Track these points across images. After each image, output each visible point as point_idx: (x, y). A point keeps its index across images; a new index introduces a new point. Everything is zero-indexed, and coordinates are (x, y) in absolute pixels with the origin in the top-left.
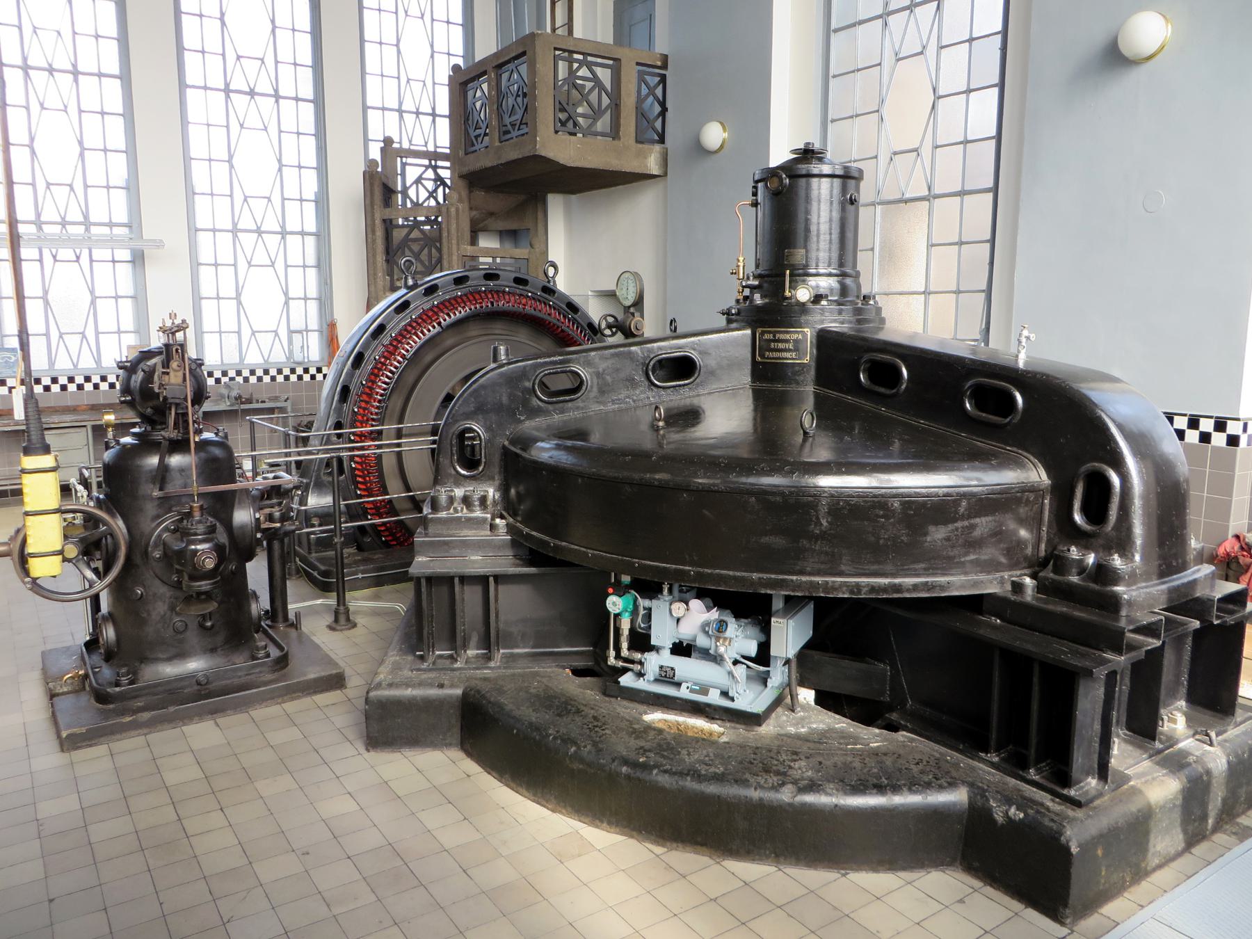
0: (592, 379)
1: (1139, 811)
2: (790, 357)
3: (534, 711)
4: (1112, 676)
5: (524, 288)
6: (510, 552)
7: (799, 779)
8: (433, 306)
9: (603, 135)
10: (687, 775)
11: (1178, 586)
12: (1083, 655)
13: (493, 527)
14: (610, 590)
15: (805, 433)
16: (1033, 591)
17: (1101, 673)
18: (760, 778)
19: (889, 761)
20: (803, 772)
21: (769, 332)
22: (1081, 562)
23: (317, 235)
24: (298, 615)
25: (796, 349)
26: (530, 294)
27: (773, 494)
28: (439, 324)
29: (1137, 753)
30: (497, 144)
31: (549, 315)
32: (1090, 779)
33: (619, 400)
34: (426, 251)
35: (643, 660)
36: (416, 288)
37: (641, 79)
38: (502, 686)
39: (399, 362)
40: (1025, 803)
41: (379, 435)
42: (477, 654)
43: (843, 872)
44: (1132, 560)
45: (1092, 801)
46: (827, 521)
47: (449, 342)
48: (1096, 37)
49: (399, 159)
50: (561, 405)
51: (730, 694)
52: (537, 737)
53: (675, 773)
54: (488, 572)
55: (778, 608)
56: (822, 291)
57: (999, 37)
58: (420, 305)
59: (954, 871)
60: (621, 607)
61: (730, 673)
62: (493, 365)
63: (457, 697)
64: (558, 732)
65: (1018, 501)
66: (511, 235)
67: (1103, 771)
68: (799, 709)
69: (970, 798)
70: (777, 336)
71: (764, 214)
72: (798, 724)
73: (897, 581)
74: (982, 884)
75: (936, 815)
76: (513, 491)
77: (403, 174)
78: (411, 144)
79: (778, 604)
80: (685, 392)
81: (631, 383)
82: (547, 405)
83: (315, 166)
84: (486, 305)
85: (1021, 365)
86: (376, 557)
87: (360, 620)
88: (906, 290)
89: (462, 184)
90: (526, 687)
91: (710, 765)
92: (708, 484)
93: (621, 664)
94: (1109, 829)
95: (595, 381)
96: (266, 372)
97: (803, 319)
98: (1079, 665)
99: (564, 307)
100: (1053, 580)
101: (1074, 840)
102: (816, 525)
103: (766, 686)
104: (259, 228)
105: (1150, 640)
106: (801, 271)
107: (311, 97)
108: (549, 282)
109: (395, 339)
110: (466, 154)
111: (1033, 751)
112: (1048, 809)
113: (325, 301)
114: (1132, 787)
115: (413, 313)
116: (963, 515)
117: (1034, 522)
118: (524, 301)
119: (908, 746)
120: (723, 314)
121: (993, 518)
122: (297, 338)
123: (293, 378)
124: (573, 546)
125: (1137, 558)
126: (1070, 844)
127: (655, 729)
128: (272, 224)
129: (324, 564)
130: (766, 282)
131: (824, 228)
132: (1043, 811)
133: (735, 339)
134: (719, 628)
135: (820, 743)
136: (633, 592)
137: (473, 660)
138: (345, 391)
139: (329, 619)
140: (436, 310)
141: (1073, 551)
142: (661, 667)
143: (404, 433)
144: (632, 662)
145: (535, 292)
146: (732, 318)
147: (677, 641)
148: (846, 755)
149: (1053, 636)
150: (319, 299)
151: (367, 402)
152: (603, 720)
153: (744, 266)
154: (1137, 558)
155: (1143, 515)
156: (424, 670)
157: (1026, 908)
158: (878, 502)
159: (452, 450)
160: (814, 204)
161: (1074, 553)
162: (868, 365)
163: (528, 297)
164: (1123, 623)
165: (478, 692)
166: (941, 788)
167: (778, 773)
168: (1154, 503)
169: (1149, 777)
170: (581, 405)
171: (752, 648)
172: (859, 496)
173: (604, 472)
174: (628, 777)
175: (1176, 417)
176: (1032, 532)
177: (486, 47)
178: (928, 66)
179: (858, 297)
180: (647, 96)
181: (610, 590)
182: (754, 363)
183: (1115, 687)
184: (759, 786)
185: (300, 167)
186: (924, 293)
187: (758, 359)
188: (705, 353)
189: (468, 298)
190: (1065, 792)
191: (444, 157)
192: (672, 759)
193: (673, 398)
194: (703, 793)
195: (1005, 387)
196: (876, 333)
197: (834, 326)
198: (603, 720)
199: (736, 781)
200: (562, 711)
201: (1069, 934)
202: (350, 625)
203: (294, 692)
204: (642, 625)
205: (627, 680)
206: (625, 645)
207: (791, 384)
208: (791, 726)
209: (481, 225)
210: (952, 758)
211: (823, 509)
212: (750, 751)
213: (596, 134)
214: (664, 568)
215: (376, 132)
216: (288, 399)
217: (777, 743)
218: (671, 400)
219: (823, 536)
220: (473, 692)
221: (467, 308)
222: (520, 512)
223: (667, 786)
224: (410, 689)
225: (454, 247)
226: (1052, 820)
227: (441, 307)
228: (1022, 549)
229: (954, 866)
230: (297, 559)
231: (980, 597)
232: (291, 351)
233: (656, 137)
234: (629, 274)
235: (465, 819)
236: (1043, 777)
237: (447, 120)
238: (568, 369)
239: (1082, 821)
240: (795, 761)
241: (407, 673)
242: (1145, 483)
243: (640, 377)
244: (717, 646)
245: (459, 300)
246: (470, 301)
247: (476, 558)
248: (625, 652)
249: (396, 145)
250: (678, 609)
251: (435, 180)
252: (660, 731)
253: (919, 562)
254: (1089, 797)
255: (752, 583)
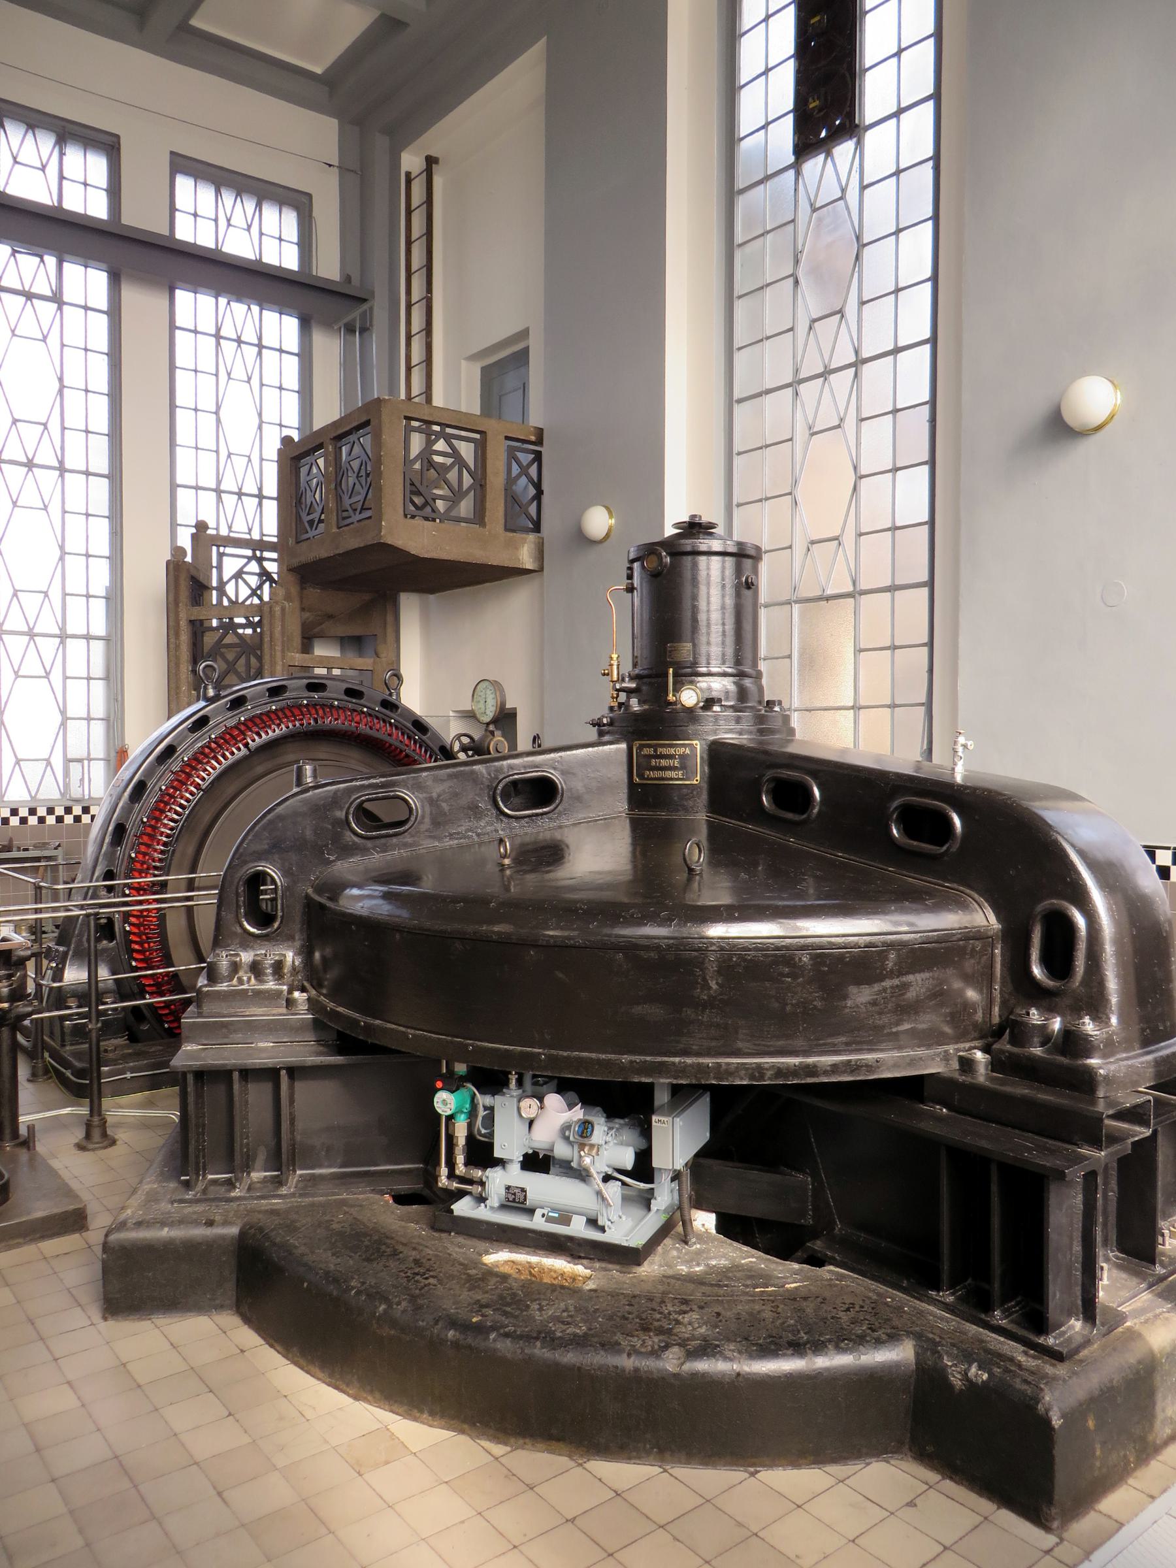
0: (423, 807)
1: (1139, 1362)
2: (675, 777)
3: (333, 1255)
4: (1091, 1176)
5: (358, 701)
6: (310, 1036)
7: (688, 1339)
8: (240, 723)
9: (466, 520)
10: (537, 1338)
11: (1168, 1056)
12: (1052, 1152)
13: (290, 1003)
14: (439, 1084)
15: (691, 870)
16: (987, 1069)
17: (1076, 1174)
18: (636, 1339)
19: (809, 1308)
20: (694, 1329)
21: (649, 746)
22: (1044, 1027)
23: (107, 639)
24: (31, 1128)
25: (683, 767)
26: (365, 709)
27: (647, 948)
28: (246, 745)
29: (1133, 1282)
30: (335, 530)
31: (390, 735)
32: (1072, 1321)
33: (458, 833)
34: (242, 661)
35: (484, 1179)
36: (218, 700)
37: (512, 456)
38: (294, 1221)
39: (192, 794)
40: (990, 1358)
41: (163, 886)
42: (265, 1177)
43: (752, 1469)
44: (1107, 1023)
45: (1077, 1351)
46: (717, 983)
47: (260, 769)
48: (1036, 408)
49: (214, 548)
50: (383, 841)
51: (600, 1223)
52: (335, 1293)
53: (521, 1337)
54: (279, 1063)
55: (662, 1103)
56: (714, 694)
57: (927, 408)
58: (222, 720)
59: (902, 1459)
60: (453, 1107)
61: (599, 1193)
62: (295, 790)
63: (232, 1238)
64: (363, 1283)
65: (962, 952)
66: (355, 643)
67: (1089, 1309)
68: (694, 1240)
69: (917, 1354)
70: (660, 750)
71: (641, 600)
72: (692, 1261)
73: (811, 1060)
74: (939, 1477)
75: (872, 1380)
76: (317, 955)
77: (220, 567)
78: (230, 531)
79: (662, 1097)
80: (545, 823)
81: (474, 811)
82: (363, 841)
83: (107, 554)
84: (309, 722)
85: (959, 779)
86: (153, 1049)
87: (122, 1136)
88: (831, 704)
89: (291, 578)
90: (327, 1221)
91: (568, 1323)
92: (560, 937)
93: (455, 1185)
94: (1101, 1390)
95: (428, 809)
96: (32, 812)
97: (691, 729)
98: (1048, 1164)
99: (410, 725)
100: (1011, 1054)
101: (1055, 1408)
102: (702, 989)
103: (649, 1209)
104: (31, 629)
105: (1137, 1128)
106: (689, 670)
107: (106, 472)
108: (391, 695)
109: (188, 764)
110: (298, 542)
111: (997, 1285)
112: (1019, 1366)
113: (114, 720)
114: (1129, 1329)
115: (213, 732)
116: (892, 971)
117: (984, 979)
118: (357, 719)
119: (836, 1285)
120: (594, 725)
121: (931, 974)
122: (75, 768)
123: (69, 819)
124: (389, 1026)
125: (1114, 1020)
126: (1051, 1413)
127: (497, 1275)
128: (48, 624)
129: (80, 1060)
130: (645, 684)
131: (715, 616)
132: (1013, 1368)
133: (608, 755)
134: (583, 1133)
135: (719, 1286)
136: (470, 1086)
137: (259, 1185)
138: (120, 830)
139: (80, 1134)
140: (242, 728)
141: (1034, 1014)
142: (508, 1188)
143: (196, 884)
144: (470, 1182)
145: (373, 706)
146: (604, 730)
147: (530, 1152)
148: (753, 1301)
149: (1014, 1127)
150: (107, 719)
151: (148, 846)
152: (427, 1265)
153: (618, 665)
154: (1114, 1020)
155: (1117, 965)
156: (190, 1202)
157: (998, 1509)
158: (783, 956)
159: (237, 901)
160: (703, 589)
161: (1035, 1017)
162: (772, 785)
163: (363, 712)
164: (1101, 1107)
165: (261, 1229)
166: (879, 1343)
167: (660, 1331)
168: (1129, 948)
169: (1150, 1315)
170: (409, 840)
171: (627, 1159)
172: (756, 949)
173: (428, 924)
174: (456, 1345)
175: (1157, 851)
176: (981, 992)
177: (328, 412)
178: (847, 441)
179: (760, 702)
180: (519, 476)
181: (439, 1084)
182: (631, 785)
183: (1096, 1193)
184: (633, 1352)
185: (88, 556)
186: (852, 708)
187: (637, 780)
188: (569, 773)
189: (284, 714)
190: (1041, 1340)
191: (271, 547)
192: (516, 1317)
193: (529, 830)
194: (557, 1364)
195: (940, 806)
196: (782, 747)
197: (730, 737)
198: (427, 1265)
199: (603, 1345)
200: (373, 1254)
201: (1057, 1544)
202: (105, 1143)
203: (12, 1238)
204: (483, 1131)
205: (463, 1208)
206: (460, 1159)
207: (678, 810)
208: (682, 1263)
209: (316, 630)
210: (893, 1300)
211: (711, 968)
212: (624, 1302)
213: (459, 520)
214: (506, 1050)
215: (187, 515)
216: (59, 846)
217: (661, 1288)
218: (526, 834)
219: (710, 1004)
220: (253, 1231)
221: (283, 726)
222: (326, 983)
223: (509, 1356)
224: (166, 1229)
225: (279, 654)
226: (1026, 1381)
227: (250, 724)
228: (970, 1015)
229: (902, 1453)
230: (46, 1055)
231: (920, 1079)
232: (67, 785)
233: (531, 526)
234: (487, 683)
235: (230, 1414)
236: (1012, 1322)
237: (275, 502)
238: (392, 794)
239: (1064, 1381)
240: (685, 1312)
241: (165, 1206)
242: (1116, 922)
243: (484, 804)
244: (581, 1156)
245: (273, 716)
246: (287, 717)
247: (266, 1044)
248: (461, 1169)
249: (209, 532)
250: (530, 1107)
251: (260, 575)
252: (505, 1277)
253: (838, 1034)
254: (1073, 1346)
255: (622, 1068)
